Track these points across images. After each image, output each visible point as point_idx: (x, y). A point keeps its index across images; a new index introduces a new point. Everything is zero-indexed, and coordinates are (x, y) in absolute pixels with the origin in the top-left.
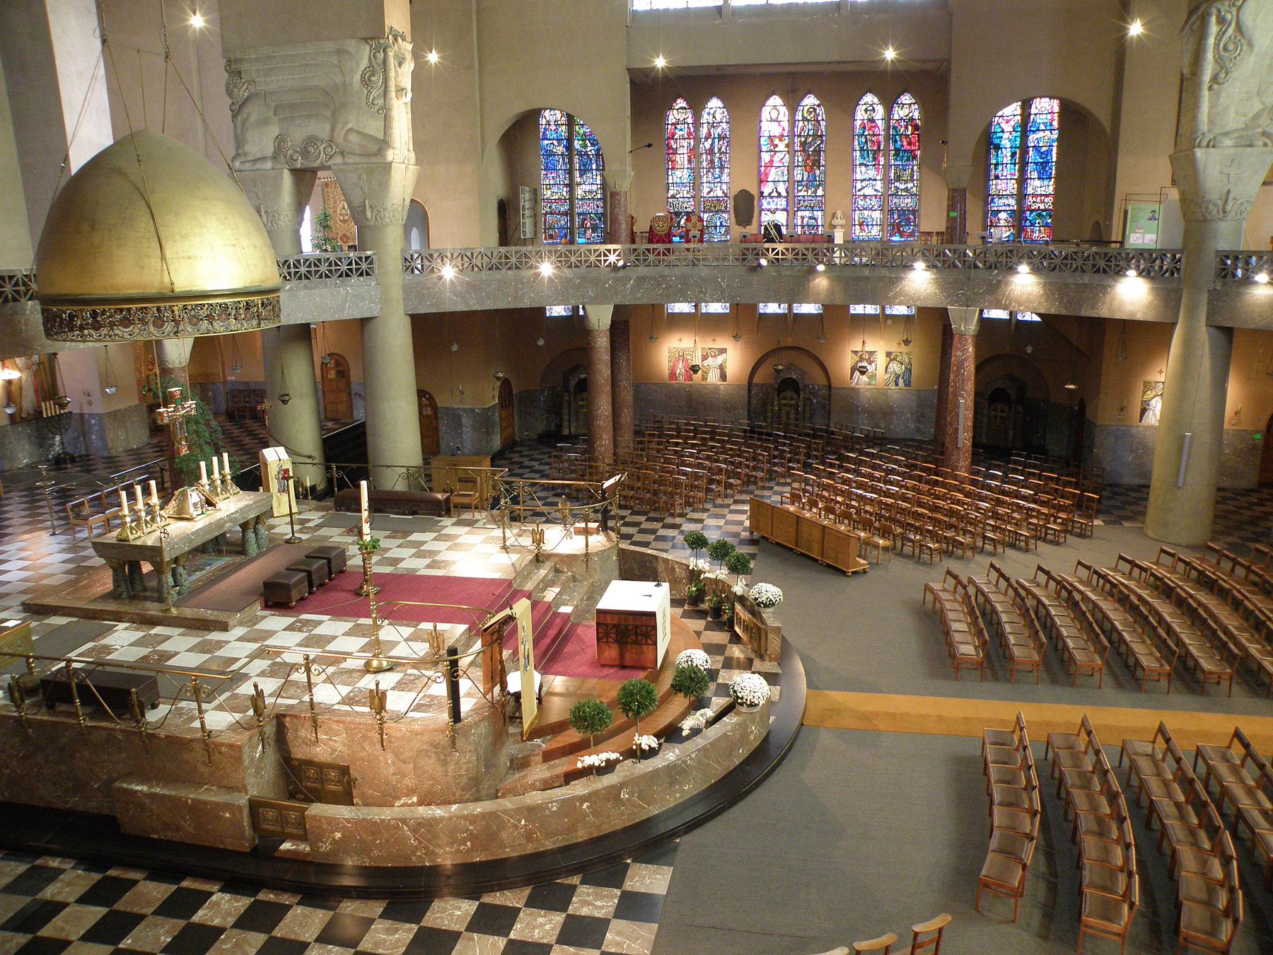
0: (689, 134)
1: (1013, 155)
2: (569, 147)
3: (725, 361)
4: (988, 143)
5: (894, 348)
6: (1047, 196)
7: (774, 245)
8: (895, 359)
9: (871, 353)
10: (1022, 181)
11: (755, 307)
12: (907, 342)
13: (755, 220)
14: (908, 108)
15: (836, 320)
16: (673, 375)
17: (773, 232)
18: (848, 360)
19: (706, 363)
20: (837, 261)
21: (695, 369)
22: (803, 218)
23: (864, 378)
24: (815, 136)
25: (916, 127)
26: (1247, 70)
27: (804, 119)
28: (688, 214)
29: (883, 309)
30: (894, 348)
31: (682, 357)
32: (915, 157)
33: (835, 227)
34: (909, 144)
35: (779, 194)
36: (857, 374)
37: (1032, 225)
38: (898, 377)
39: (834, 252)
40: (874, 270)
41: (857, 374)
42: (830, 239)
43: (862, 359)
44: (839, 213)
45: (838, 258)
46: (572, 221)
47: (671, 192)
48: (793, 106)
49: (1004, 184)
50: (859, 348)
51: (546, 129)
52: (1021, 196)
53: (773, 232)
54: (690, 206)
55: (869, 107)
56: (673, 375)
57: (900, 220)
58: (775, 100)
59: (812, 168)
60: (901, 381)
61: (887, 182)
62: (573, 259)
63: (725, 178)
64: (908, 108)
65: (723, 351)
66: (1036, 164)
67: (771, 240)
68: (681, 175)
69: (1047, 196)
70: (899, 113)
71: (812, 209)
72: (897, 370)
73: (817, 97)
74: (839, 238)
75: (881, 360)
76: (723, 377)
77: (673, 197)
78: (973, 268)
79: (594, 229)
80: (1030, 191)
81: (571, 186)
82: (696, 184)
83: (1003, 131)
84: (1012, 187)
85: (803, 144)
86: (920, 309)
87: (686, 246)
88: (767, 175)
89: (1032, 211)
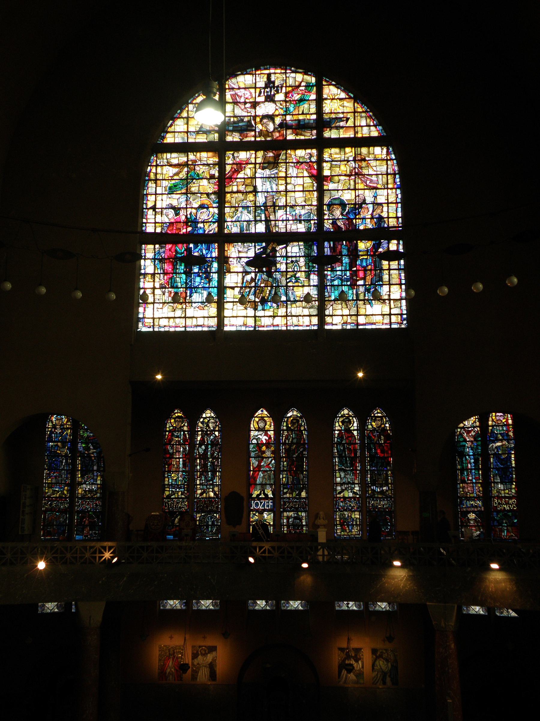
0: (185, 439)
1: (476, 462)
2: (73, 449)
3: (214, 660)
4: (455, 449)
5: (379, 645)
6: (510, 498)
7: (262, 544)
8: (381, 656)
9: (358, 650)
10: (487, 485)
11: (246, 604)
12: (390, 639)
13: (244, 520)
14: (379, 420)
15: (323, 619)
16: (162, 672)
17: (261, 531)
18: (336, 658)
19: (196, 662)
20: (320, 558)
21: (184, 668)
22: (288, 518)
23: (352, 676)
24: (298, 444)
25: (387, 437)
26: (218, 667)
27: (288, 429)
28: (181, 513)
29: (366, 606)
30: (379, 645)
31: (172, 653)
32: (388, 463)
33: (318, 527)
34: (383, 451)
35: (266, 495)
36: (344, 672)
37: (501, 524)
38: (384, 674)
39: (318, 550)
40: (359, 565)
41: (344, 672)
42: (314, 537)
43: (348, 657)
44: (322, 514)
45: (322, 555)
46: (71, 519)
47: (167, 493)
48: (278, 417)
49: (471, 486)
50: (344, 645)
51: (51, 432)
52: (487, 497)
53: (261, 531)
54: (184, 506)
55: (346, 422)
56: (162, 672)
57: (373, 521)
58: (262, 412)
59: (295, 472)
60: (388, 679)
61: (364, 485)
62: (69, 555)
63: (217, 481)
64: (379, 420)
65: (212, 649)
66: (497, 469)
67: (259, 539)
68: (175, 477)
69: (510, 498)
70: (372, 425)
71: (297, 510)
72: (384, 667)
73: (299, 410)
74: (322, 537)
75: (367, 657)
76: (213, 675)
77: (169, 497)
78: (448, 565)
79: (92, 526)
80: (494, 492)
81: (73, 486)
82: (191, 486)
83: (465, 441)
84: (478, 489)
85: (287, 451)
86: (401, 606)
87: (179, 543)
88: (255, 479)
89: (498, 512)
